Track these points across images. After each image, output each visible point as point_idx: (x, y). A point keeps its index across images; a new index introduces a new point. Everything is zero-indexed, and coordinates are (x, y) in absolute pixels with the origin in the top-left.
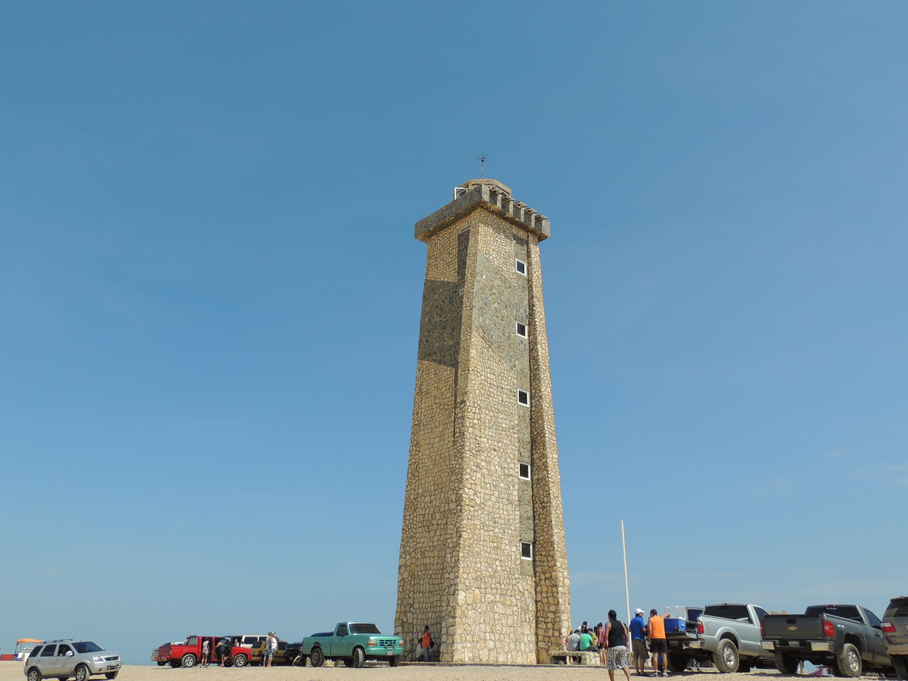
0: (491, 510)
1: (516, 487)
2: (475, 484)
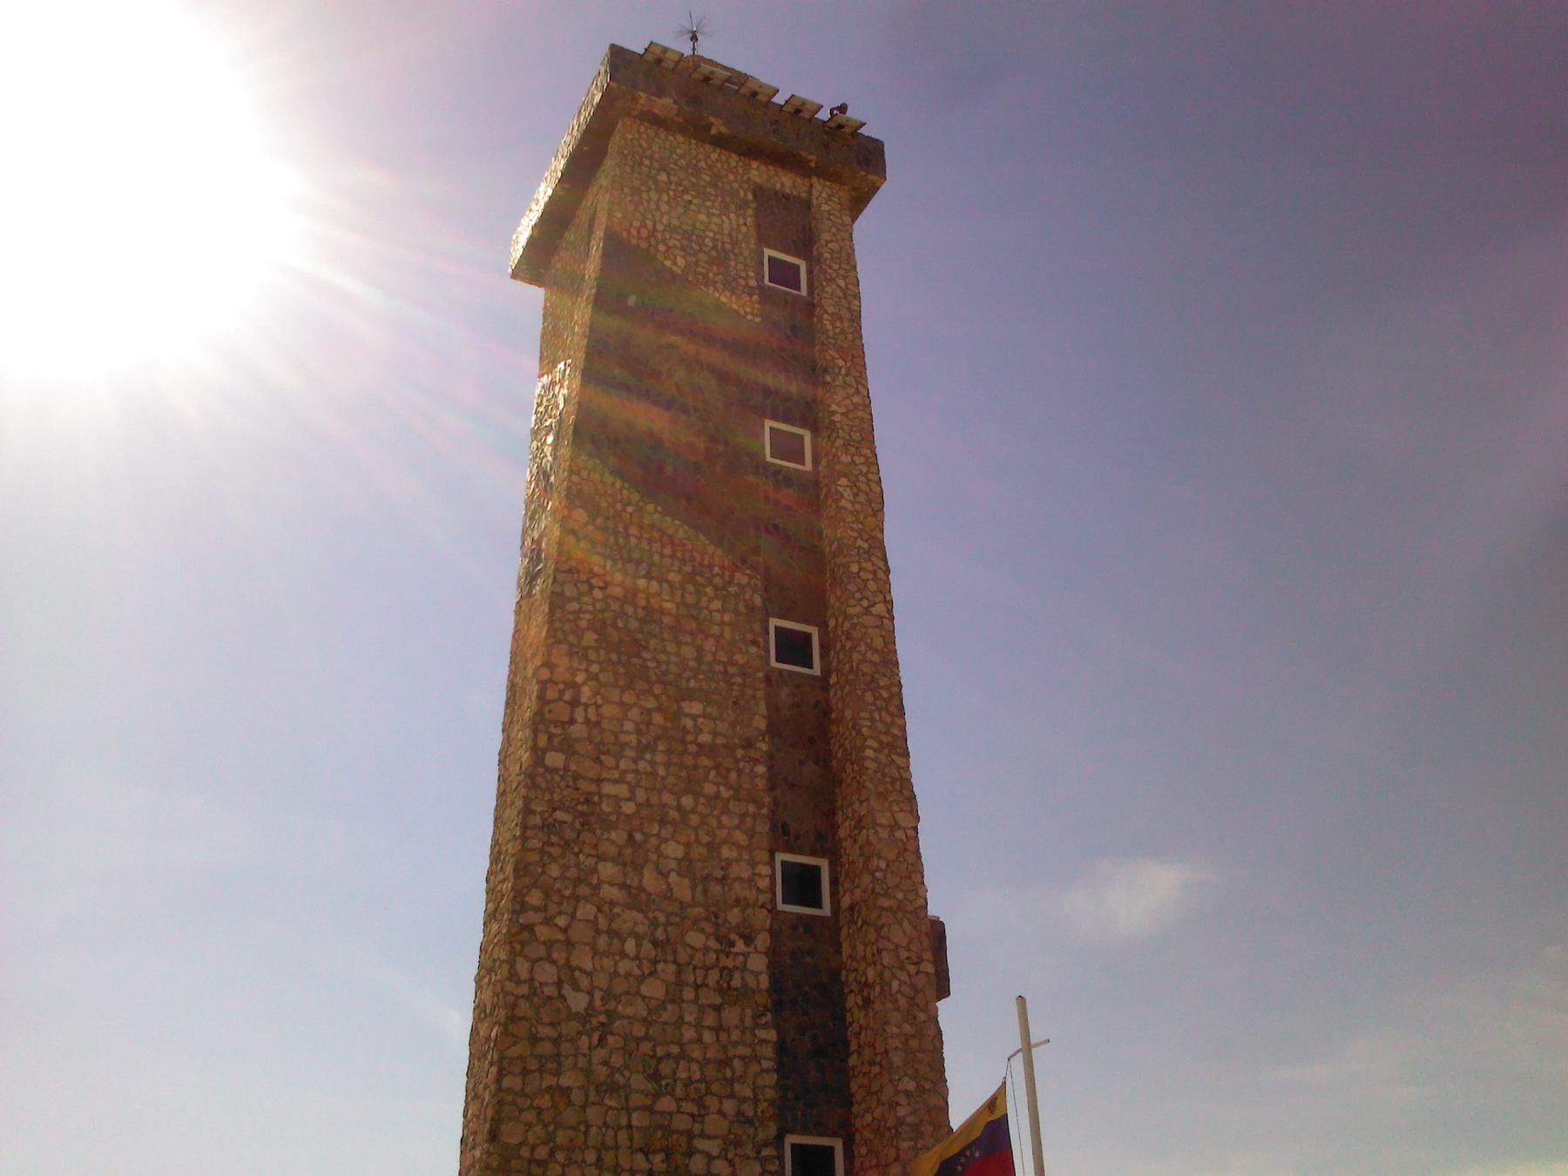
0: (639, 1031)
1: (762, 940)
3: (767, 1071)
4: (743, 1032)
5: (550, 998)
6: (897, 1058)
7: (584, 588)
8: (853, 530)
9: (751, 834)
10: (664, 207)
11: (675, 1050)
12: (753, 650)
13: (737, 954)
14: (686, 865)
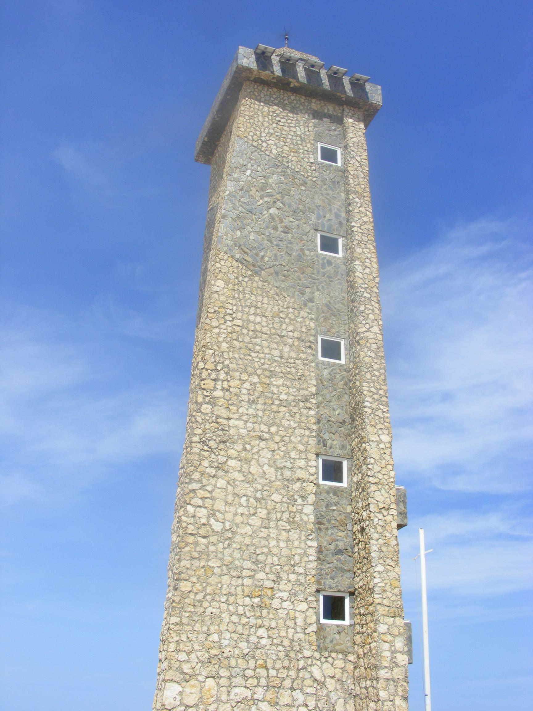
0: (247, 541)
1: (311, 499)
2: (213, 499)
5: (204, 524)
7: (222, 322)
8: (362, 288)
10: (266, 124)
11: (265, 550)
12: (309, 351)
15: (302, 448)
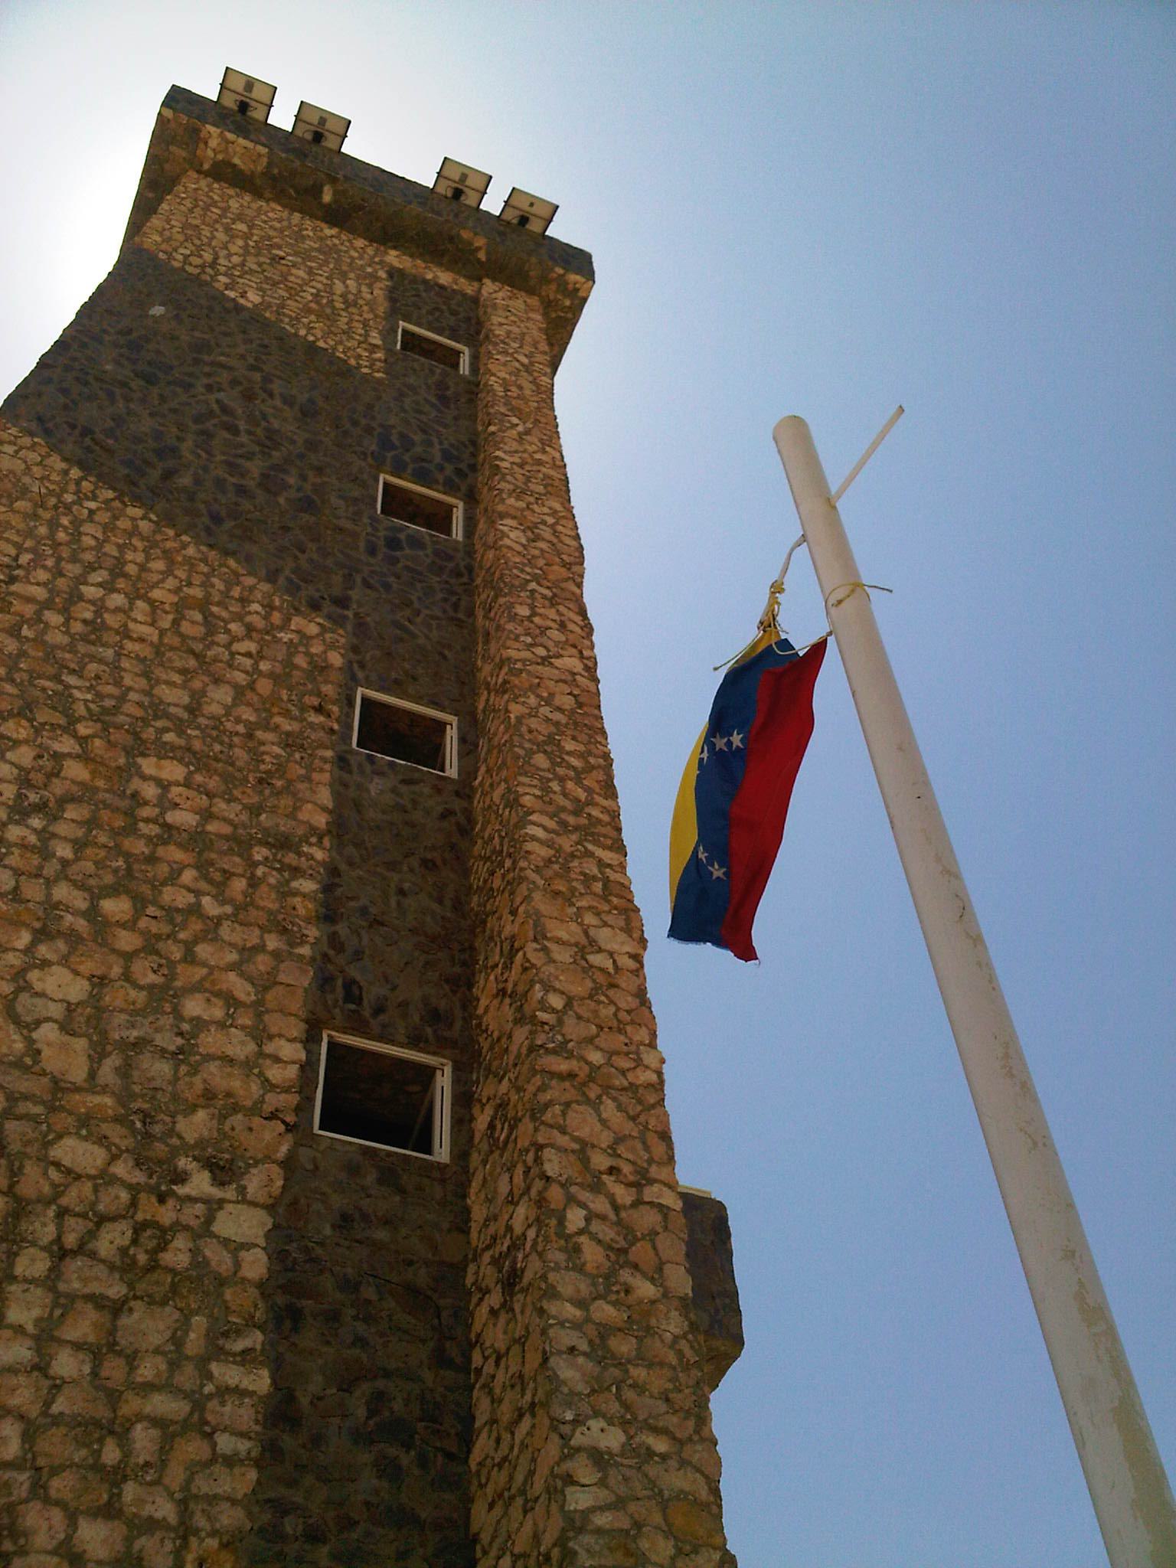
3: (231, 1461)
4: (174, 1365)
6: (570, 1373)
9: (266, 984)
13: (191, 1199)
14: (86, 1020)
15: (243, 990)
